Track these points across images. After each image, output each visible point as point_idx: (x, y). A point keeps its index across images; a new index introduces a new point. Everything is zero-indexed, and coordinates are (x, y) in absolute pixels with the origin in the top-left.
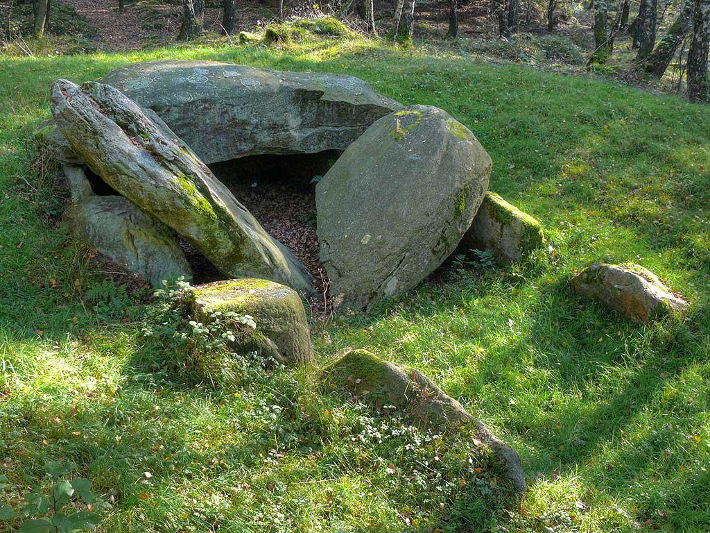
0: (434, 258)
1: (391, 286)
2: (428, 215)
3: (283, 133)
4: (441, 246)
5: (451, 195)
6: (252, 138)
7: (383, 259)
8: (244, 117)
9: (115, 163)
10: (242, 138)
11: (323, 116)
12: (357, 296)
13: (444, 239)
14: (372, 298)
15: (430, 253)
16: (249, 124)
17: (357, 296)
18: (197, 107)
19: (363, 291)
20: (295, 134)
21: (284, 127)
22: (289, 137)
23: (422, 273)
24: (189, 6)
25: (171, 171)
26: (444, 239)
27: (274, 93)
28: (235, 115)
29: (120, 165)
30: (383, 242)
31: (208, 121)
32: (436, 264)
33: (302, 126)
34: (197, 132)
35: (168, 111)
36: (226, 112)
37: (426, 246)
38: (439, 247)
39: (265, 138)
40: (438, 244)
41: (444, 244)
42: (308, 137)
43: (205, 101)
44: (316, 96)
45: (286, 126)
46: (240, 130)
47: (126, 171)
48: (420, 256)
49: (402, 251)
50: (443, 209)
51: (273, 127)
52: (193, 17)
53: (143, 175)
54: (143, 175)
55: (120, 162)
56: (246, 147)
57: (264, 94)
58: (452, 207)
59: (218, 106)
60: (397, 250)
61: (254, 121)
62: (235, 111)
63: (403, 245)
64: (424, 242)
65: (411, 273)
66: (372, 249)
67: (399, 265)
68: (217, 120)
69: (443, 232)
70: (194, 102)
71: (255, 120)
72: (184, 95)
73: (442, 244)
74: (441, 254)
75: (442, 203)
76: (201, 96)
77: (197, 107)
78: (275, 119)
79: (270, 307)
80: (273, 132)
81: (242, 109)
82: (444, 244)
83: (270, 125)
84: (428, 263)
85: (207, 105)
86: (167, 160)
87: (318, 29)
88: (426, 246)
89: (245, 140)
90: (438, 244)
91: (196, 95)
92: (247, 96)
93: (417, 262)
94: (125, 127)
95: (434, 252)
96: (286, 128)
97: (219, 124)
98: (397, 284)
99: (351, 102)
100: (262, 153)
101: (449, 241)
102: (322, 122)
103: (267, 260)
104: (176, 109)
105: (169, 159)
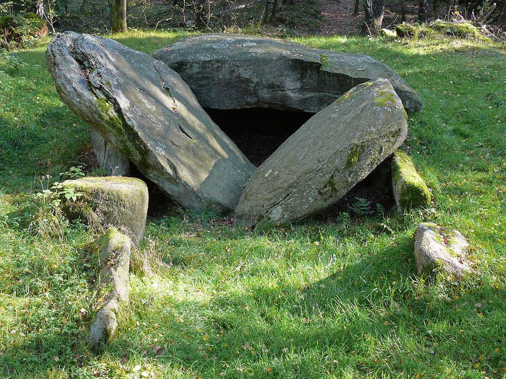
0: (319, 197)
1: (277, 214)
2: (319, 162)
3: (280, 92)
4: (327, 189)
5: (346, 148)
6: (255, 93)
7: (274, 190)
8: (247, 77)
9: (59, 84)
10: (247, 92)
11: (325, 83)
12: (250, 216)
13: (331, 183)
14: (260, 219)
15: (316, 193)
16: (252, 82)
17: (250, 216)
18: (212, 65)
19: (255, 213)
20: (292, 95)
21: (281, 87)
22: (286, 96)
23: (304, 209)
24: (369, 9)
25: (95, 94)
26: (331, 183)
27: (272, 60)
28: (240, 74)
29: (62, 86)
30: (278, 177)
31: (221, 77)
32: (321, 204)
33: (302, 90)
34: (214, 84)
35: (191, 66)
36: (233, 71)
37: (313, 187)
38: (325, 190)
39: (265, 94)
40: (325, 187)
41: (330, 188)
42: (306, 99)
43: (218, 61)
44: (316, 67)
45: (282, 87)
46: (245, 86)
47: (63, 90)
48: (305, 194)
49: (291, 186)
50: (335, 159)
51: (271, 86)
52: (371, 18)
53: (73, 95)
54: (73, 95)
55: (63, 84)
56: (252, 100)
57: (264, 60)
58: (345, 159)
59: (227, 65)
60: (285, 185)
61: (255, 80)
62: (240, 71)
63: (291, 181)
64: (310, 183)
65: (294, 206)
66: (269, 181)
67: (286, 197)
68: (228, 76)
69: (332, 177)
70: (210, 61)
71: (256, 79)
72: (205, 56)
73: (329, 188)
74: (326, 197)
75: (335, 153)
76: (215, 57)
77: (212, 65)
78: (272, 80)
79: (103, 193)
80: (272, 91)
81: (245, 70)
82: (330, 188)
83: (268, 84)
84: (311, 201)
85: (219, 65)
86: (94, 86)
87: (449, 31)
88: (313, 187)
89: (251, 95)
90: (325, 187)
91: (213, 57)
92: (249, 61)
93: (302, 197)
94: (80, 62)
95: (320, 193)
96: (282, 88)
97: (229, 80)
98: (282, 213)
99: (350, 75)
100: (266, 106)
101: (336, 186)
102: (323, 89)
103: (170, 171)
104: (197, 65)
105: (95, 86)
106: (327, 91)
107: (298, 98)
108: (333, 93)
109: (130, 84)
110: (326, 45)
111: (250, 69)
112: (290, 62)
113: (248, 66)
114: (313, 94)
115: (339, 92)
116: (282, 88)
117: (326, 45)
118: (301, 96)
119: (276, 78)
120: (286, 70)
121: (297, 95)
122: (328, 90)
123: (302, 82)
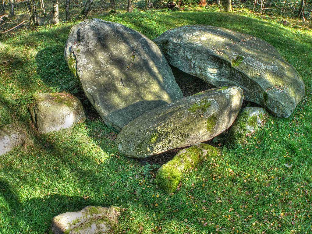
11: (235, 76)
96: (205, 71)
102: (234, 79)
106: (235, 81)
107: (215, 80)
108: (239, 84)
109: (72, 26)
110: (236, 109)
111: (191, 54)
112: (211, 56)
113: (190, 52)
114: (226, 80)
115: (242, 84)
116: (205, 71)
117: (236, 109)
118: (218, 79)
119: (202, 64)
120: (209, 60)
121: (215, 77)
122: (237, 81)
123: (220, 70)
